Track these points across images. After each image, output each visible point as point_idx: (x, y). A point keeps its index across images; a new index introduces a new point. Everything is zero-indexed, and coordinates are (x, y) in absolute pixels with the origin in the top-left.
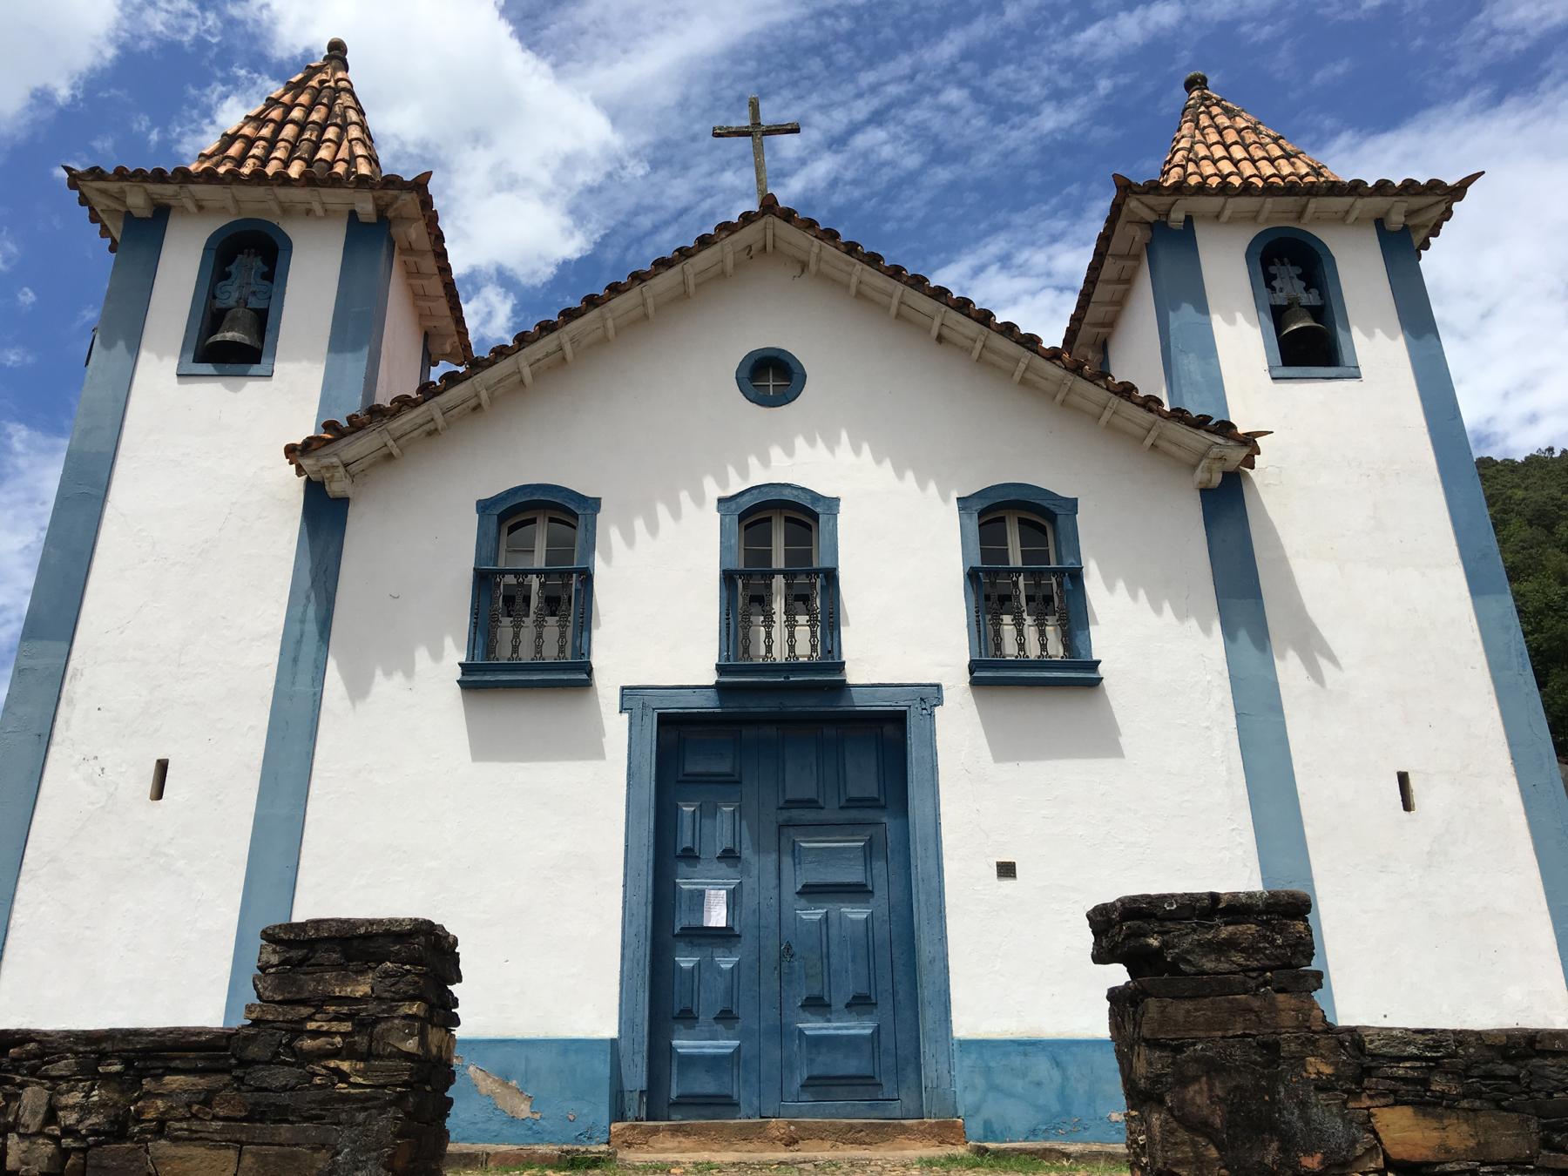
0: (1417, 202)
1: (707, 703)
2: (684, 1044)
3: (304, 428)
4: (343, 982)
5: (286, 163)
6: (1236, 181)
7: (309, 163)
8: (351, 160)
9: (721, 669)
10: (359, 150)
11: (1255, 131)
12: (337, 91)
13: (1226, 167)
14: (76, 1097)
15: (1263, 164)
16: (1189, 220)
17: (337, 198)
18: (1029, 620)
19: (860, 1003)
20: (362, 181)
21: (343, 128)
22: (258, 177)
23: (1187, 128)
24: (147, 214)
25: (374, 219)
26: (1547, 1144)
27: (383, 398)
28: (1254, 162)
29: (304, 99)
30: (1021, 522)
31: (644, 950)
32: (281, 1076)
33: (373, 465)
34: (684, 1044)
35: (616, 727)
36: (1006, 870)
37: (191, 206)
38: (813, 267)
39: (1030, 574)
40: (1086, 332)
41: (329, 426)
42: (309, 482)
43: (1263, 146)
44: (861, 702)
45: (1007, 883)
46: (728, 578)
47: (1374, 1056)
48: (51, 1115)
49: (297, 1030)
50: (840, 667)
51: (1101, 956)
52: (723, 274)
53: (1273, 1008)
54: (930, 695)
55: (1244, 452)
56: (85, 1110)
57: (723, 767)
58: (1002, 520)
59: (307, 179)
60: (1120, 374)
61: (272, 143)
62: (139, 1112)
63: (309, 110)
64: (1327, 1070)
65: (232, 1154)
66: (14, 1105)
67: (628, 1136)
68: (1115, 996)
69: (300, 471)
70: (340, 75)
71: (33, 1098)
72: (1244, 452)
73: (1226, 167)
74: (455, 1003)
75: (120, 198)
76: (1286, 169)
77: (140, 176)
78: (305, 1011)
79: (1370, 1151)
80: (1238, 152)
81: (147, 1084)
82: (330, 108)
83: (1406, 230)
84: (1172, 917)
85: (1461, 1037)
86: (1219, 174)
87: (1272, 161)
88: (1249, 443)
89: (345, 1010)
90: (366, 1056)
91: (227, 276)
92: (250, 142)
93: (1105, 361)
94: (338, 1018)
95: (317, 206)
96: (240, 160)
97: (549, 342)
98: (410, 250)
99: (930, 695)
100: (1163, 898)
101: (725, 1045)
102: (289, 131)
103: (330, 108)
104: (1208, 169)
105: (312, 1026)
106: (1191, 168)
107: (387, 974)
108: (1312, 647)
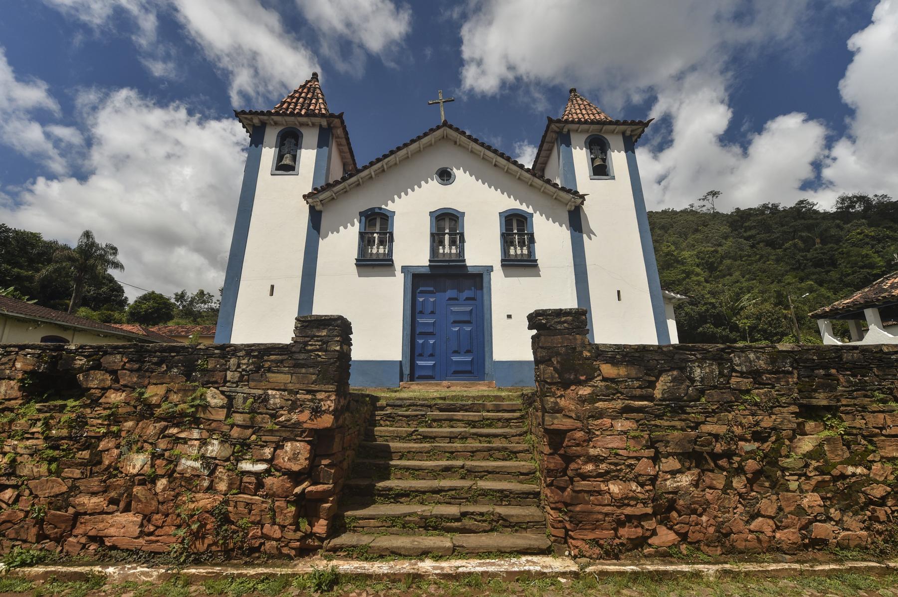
0: (634, 127)
1: (427, 271)
2: (420, 363)
3: (309, 189)
4: (319, 331)
5: (301, 110)
6: (583, 120)
7: (307, 110)
8: (320, 109)
9: (430, 261)
10: (322, 106)
11: (590, 106)
12: (315, 88)
13: (580, 116)
14: (245, 361)
15: (591, 115)
16: (569, 131)
17: (317, 120)
18: (519, 248)
19: (468, 352)
20: (323, 115)
21: (317, 100)
22: (292, 114)
23: (569, 104)
24: (259, 125)
25: (327, 127)
26: (646, 374)
27: (331, 181)
28: (588, 115)
29: (305, 90)
30: (517, 220)
31: (409, 337)
32: (302, 356)
33: (329, 201)
34: (420, 363)
35: (399, 278)
36: (509, 317)
37: (272, 123)
38: (458, 143)
39: (519, 235)
40: (538, 166)
41: (315, 189)
42: (310, 206)
43: (591, 110)
44: (470, 271)
45: (509, 320)
46: (432, 235)
47: (602, 351)
48: (239, 366)
49: (306, 344)
50: (464, 261)
51: (530, 328)
52: (431, 145)
53: (575, 339)
54: (490, 269)
55: (580, 200)
56: (248, 364)
57: (432, 289)
58: (512, 219)
59: (306, 115)
60: (547, 177)
61: (296, 104)
62: (263, 365)
63: (307, 94)
64: (588, 354)
65: (290, 376)
66: (228, 363)
67: (405, 386)
68: (533, 337)
69: (307, 203)
70: (316, 83)
71: (233, 361)
72: (580, 200)
73: (580, 116)
74: (351, 339)
75: (251, 120)
76: (598, 117)
77: (256, 113)
78: (308, 339)
79: (599, 375)
80: (584, 112)
81: (266, 358)
82: (313, 93)
83: (631, 136)
84: (549, 315)
85: (625, 346)
86: (578, 118)
87: (593, 114)
88: (582, 197)
89: (319, 339)
90: (326, 351)
91: (284, 144)
92: (289, 104)
93: (544, 174)
94: (317, 341)
95: (310, 123)
96: (287, 109)
97: (379, 165)
98: (338, 137)
99: (490, 269)
100: (546, 310)
101: (431, 363)
102: (301, 100)
103: (313, 93)
104: (575, 116)
105: (310, 343)
106: (570, 116)
107: (331, 329)
108: (590, 233)
